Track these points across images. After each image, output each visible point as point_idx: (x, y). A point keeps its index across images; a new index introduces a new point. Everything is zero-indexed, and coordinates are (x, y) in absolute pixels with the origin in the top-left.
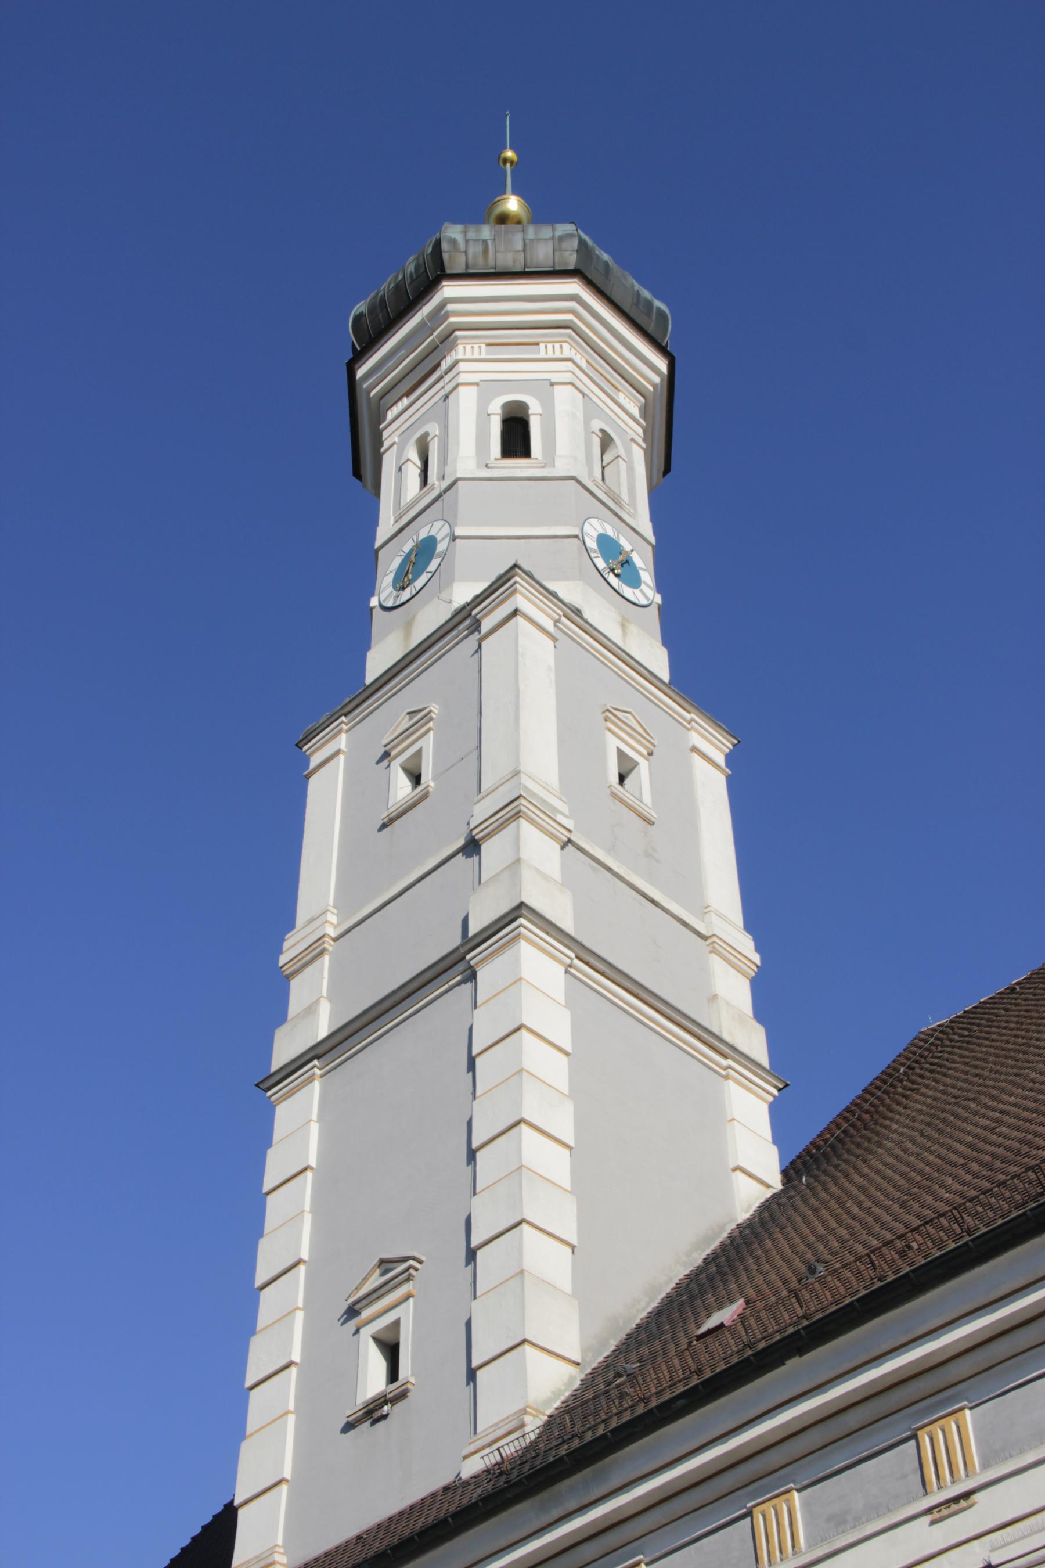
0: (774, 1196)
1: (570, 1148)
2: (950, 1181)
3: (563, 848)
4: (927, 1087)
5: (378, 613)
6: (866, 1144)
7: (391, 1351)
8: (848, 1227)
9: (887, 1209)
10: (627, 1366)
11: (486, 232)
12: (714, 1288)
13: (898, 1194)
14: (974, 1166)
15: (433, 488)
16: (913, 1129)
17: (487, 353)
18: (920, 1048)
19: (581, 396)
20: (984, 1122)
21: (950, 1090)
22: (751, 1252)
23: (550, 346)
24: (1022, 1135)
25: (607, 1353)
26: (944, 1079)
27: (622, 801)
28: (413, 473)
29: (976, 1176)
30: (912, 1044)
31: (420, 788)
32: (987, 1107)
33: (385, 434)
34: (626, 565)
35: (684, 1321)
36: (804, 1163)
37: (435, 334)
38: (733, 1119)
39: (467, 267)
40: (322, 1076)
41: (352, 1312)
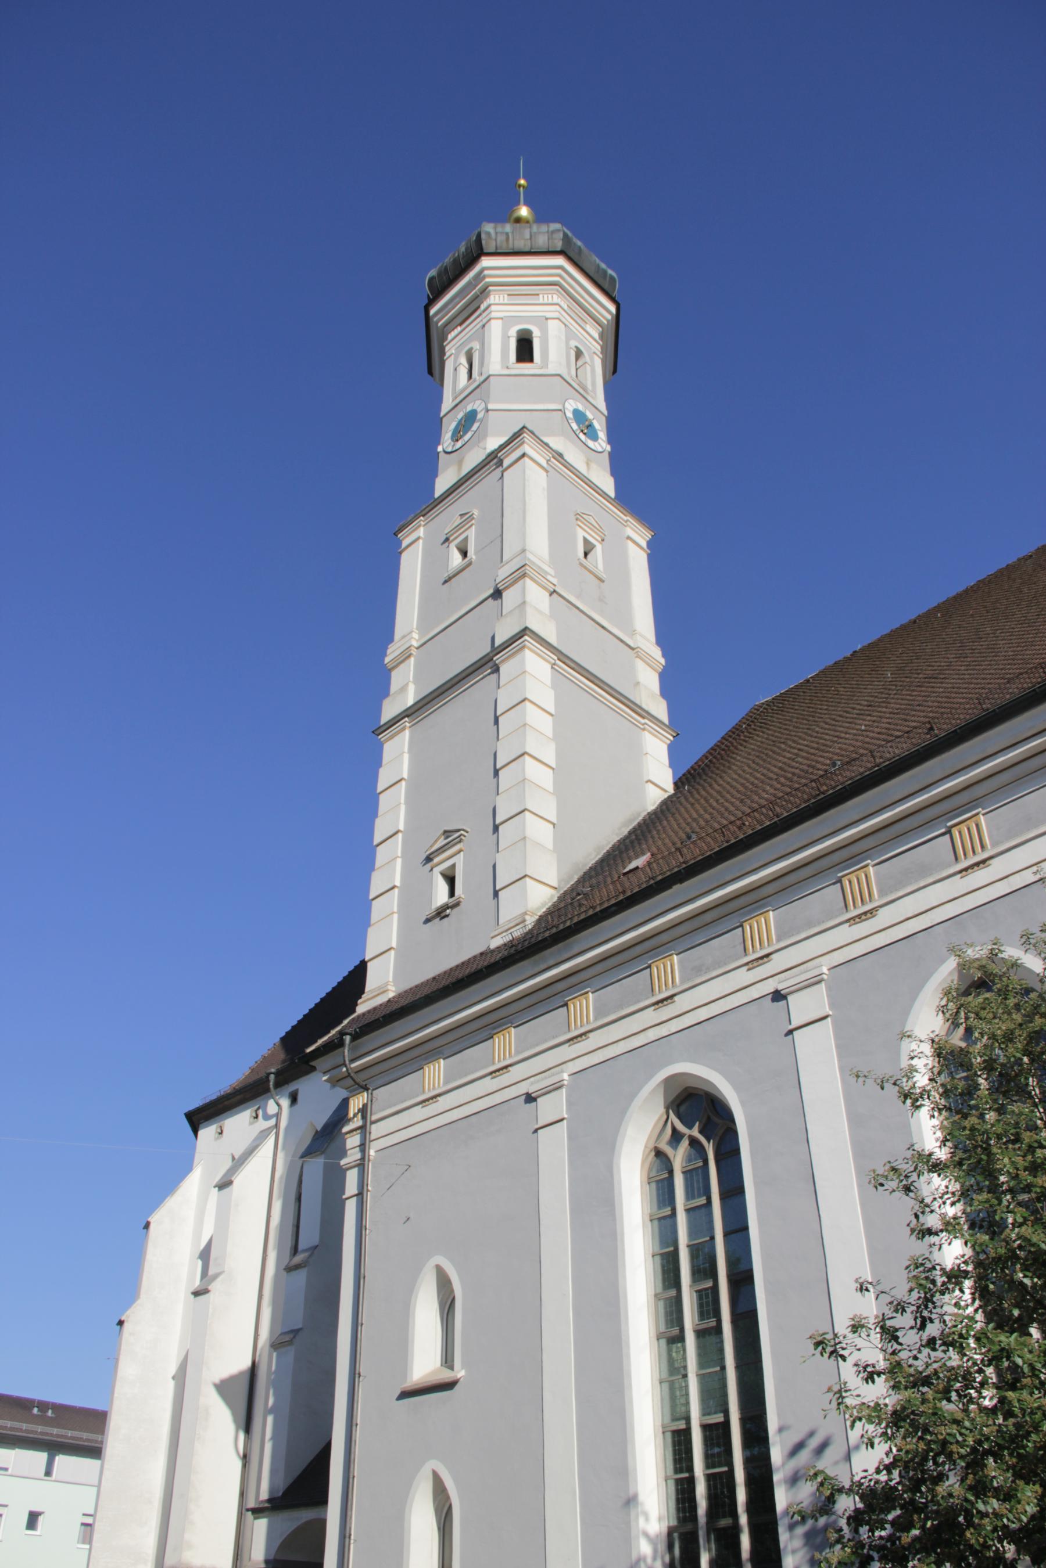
0: (670, 797)
1: (553, 769)
2: (768, 788)
3: (551, 595)
4: (758, 735)
5: (442, 456)
6: (722, 768)
7: (451, 881)
8: (710, 814)
9: (732, 804)
10: (584, 890)
11: (508, 228)
12: (633, 847)
13: (739, 796)
14: (782, 780)
15: (475, 381)
16: (749, 759)
17: (508, 300)
18: (755, 714)
19: (564, 326)
20: (788, 755)
21: (771, 737)
22: (655, 828)
23: (546, 296)
24: (809, 762)
25: (572, 883)
26: (767, 731)
27: (586, 568)
28: (463, 372)
29: (783, 785)
30: (750, 712)
31: (467, 560)
32: (791, 747)
33: (447, 349)
34: (589, 428)
35: (616, 865)
36: (687, 779)
37: (477, 288)
38: (647, 754)
39: (496, 248)
40: (410, 727)
41: (429, 859)
